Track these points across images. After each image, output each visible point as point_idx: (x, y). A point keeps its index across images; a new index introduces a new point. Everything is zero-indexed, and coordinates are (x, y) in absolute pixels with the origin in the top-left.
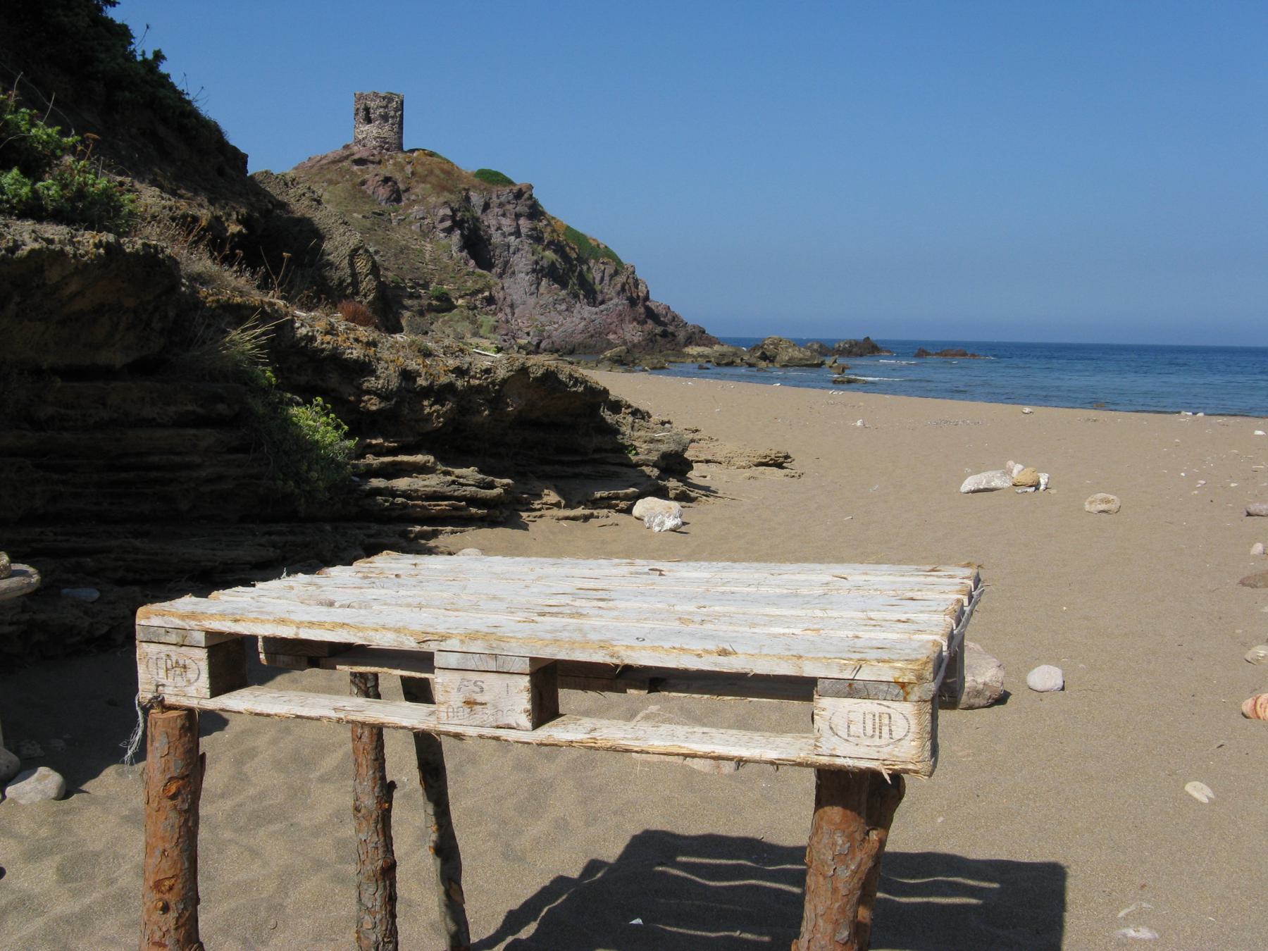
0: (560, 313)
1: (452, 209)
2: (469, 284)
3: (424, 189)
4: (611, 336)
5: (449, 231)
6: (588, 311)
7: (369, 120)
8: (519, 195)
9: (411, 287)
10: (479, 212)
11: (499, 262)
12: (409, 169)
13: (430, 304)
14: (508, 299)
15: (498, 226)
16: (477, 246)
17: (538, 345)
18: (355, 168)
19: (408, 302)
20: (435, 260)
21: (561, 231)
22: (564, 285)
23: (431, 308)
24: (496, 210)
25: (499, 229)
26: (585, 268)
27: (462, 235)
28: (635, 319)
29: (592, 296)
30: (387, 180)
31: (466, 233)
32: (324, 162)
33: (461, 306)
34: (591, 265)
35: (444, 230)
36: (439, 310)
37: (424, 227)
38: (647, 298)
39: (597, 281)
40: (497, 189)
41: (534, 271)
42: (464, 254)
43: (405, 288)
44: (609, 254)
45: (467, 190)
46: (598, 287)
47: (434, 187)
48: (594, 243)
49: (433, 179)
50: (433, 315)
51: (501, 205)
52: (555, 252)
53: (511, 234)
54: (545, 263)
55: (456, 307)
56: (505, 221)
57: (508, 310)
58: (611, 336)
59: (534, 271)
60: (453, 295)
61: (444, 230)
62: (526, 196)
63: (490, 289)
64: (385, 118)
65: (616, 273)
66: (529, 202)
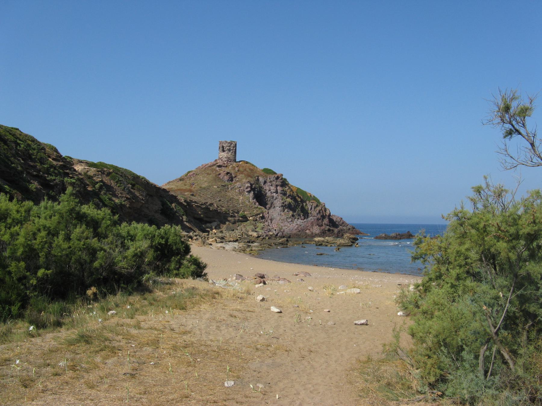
1: (251, 184)
5: (249, 192)
7: (224, 151)
8: (277, 178)
11: (269, 203)
14: (270, 217)
15: (269, 190)
16: (260, 198)
19: (230, 219)
23: (239, 221)
27: (254, 193)
30: (228, 173)
31: (256, 192)
35: (247, 192)
36: (242, 221)
41: (282, 206)
42: (255, 200)
44: (315, 199)
45: (258, 177)
46: (309, 212)
49: (245, 172)
50: (239, 223)
52: (291, 199)
54: (287, 203)
57: (269, 221)
58: (307, 231)
59: (282, 206)
60: (248, 215)
61: (247, 192)
63: (263, 213)
64: (229, 150)
65: (317, 206)
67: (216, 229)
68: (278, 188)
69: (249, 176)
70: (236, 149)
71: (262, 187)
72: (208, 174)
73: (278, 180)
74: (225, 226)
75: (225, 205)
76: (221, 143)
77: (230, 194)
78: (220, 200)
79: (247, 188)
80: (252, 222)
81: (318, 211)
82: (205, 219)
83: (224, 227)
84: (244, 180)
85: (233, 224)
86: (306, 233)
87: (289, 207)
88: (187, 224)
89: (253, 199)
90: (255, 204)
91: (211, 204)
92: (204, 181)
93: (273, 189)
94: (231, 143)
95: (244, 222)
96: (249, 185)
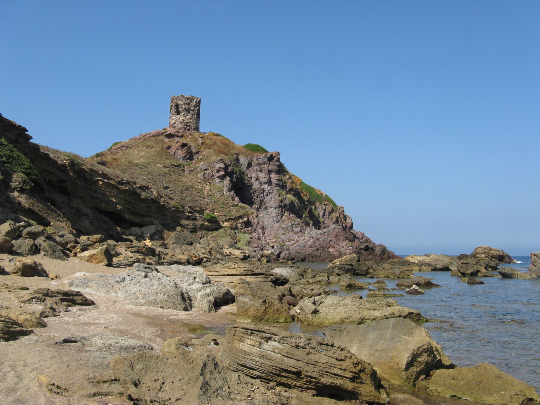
0: (296, 233)
1: (225, 164)
2: (233, 212)
3: (208, 152)
4: (331, 250)
5: (222, 178)
6: (312, 232)
7: (178, 113)
8: (271, 158)
9: (190, 212)
10: (245, 169)
11: (257, 201)
12: (200, 141)
13: (203, 225)
14: (261, 224)
15: (257, 178)
16: (241, 189)
17: (279, 255)
18: (166, 139)
19: (185, 222)
20: (210, 196)
21: (298, 183)
22: (300, 217)
23: (203, 227)
24: (256, 167)
25: (257, 179)
26: (313, 207)
27: (231, 181)
28: (347, 238)
29: (317, 224)
30: (184, 145)
31: (234, 180)
32: (148, 136)
33: (226, 227)
34: (317, 205)
35: (219, 177)
36: (208, 229)
37: (206, 176)
38: (351, 227)
39: (321, 216)
40: (256, 155)
41: (280, 206)
42: (232, 193)
43: (183, 212)
44: (328, 199)
45: (238, 155)
46: (321, 220)
47: (215, 151)
48: (319, 193)
49: (216, 148)
50: (204, 232)
51: (259, 164)
52: (294, 195)
53: (265, 183)
54: (287, 202)
55: (222, 227)
56: (261, 175)
57: (260, 231)
58: (331, 250)
59: (280, 206)
60: (220, 219)
61: (219, 177)
62: (276, 159)
63: (248, 216)
64: (188, 110)
65: (333, 211)
66: (277, 163)
67: (152, 238)
69: (221, 152)
70: (199, 110)
71: (243, 173)
72: (148, 147)
73: (272, 163)
74: (173, 234)
75: (177, 196)
76: (173, 99)
77: (187, 179)
78: (166, 188)
79: (218, 171)
80: (229, 231)
81: (334, 220)
82: (128, 217)
83: (171, 237)
84: (213, 158)
85: (191, 232)
86: (329, 254)
87: (291, 208)
88: (23, 200)
89: (230, 191)
90: (233, 199)
91: (144, 188)
92: (139, 156)
93: (263, 176)
94: (191, 99)
95: (213, 230)
96: (222, 165)
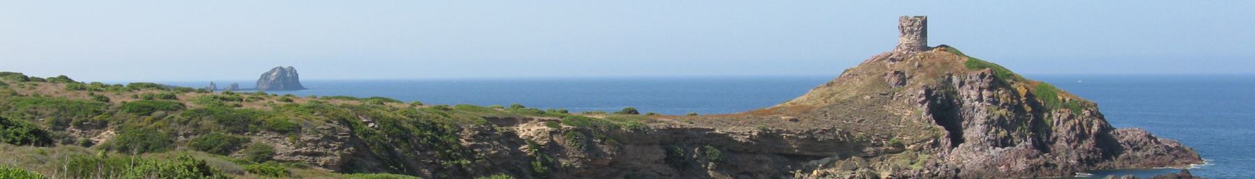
30: (896, 73)
54: (995, 118)
68: (984, 92)
94: (913, 21)
